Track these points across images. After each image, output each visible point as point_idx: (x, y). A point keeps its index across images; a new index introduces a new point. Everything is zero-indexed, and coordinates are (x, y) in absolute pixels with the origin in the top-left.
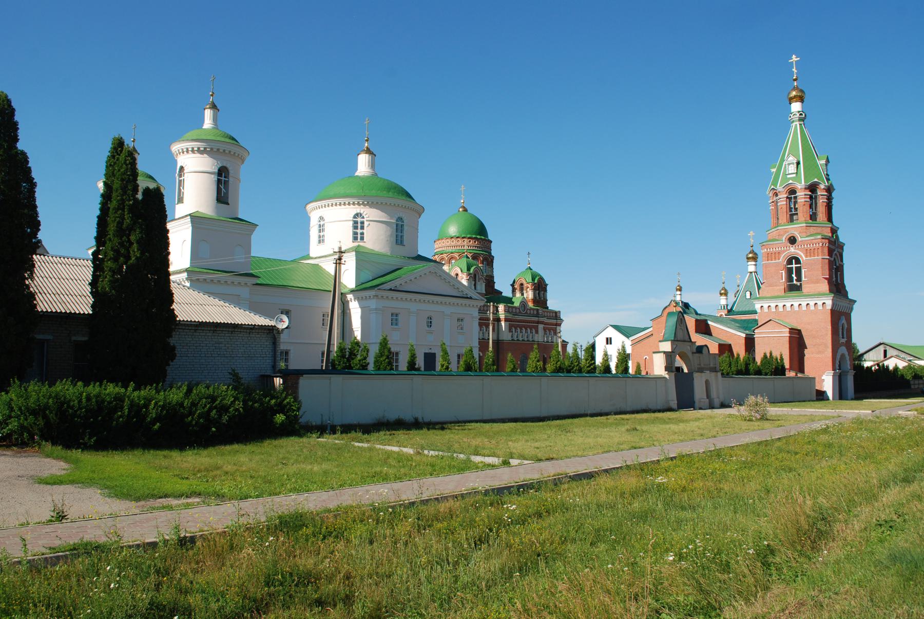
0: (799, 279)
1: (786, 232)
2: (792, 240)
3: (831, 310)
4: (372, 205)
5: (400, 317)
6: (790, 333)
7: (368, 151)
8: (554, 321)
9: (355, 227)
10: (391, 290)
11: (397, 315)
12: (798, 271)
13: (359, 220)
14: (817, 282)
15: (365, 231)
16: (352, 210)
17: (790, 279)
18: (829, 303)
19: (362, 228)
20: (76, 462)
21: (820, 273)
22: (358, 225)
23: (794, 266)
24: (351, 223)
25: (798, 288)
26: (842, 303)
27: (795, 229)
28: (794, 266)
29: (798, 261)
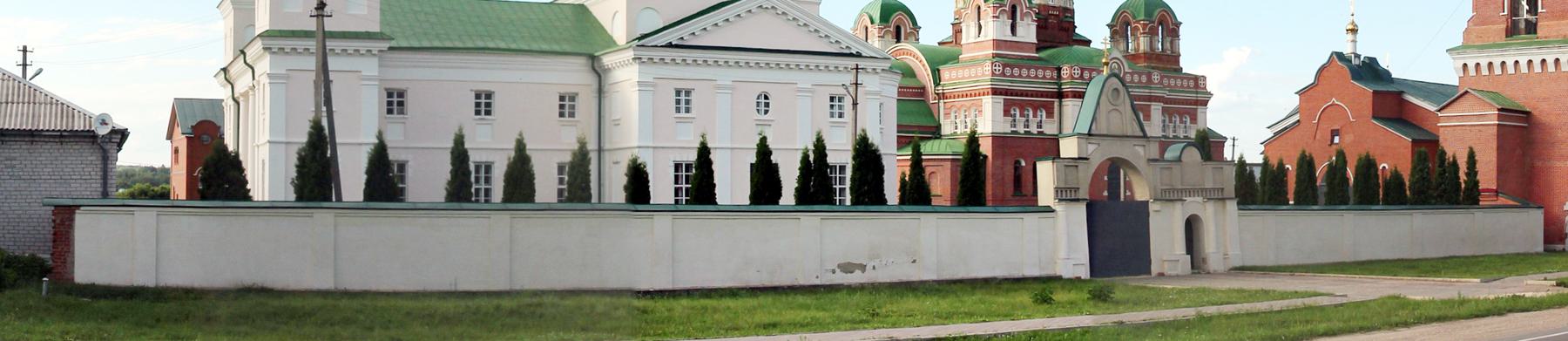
5: (693, 97)
6: (1500, 117)
8: (1192, 96)
10: (670, 45)
11: (688, 93)
25: (1531, 28)
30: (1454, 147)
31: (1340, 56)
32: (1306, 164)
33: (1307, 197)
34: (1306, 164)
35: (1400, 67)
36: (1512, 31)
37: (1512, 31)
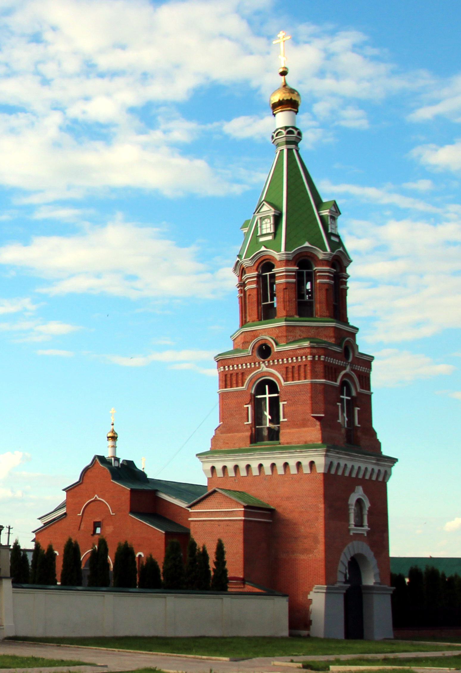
0: (275, 418)
1: (255, 337)
2: (264, 351)
3: (327, 476)
6: (246, 514)
12: (274, 403)
14: (304, 424)
17: (258, 418)
18: (320, 461)
20: (84, 112)
21: (308, 408)
23: (267, 396)
25: (274, 435)
26: (356, 464)
27: (267, 330)
28: (267, 396)
29: (273, 389)
30: (204, 540)
31: (102, 459)
32: (72, 550)
33: (73, 579)
34: (72, 550)
35: (157, 467)
36: (256, 438)
37: (256, 438)
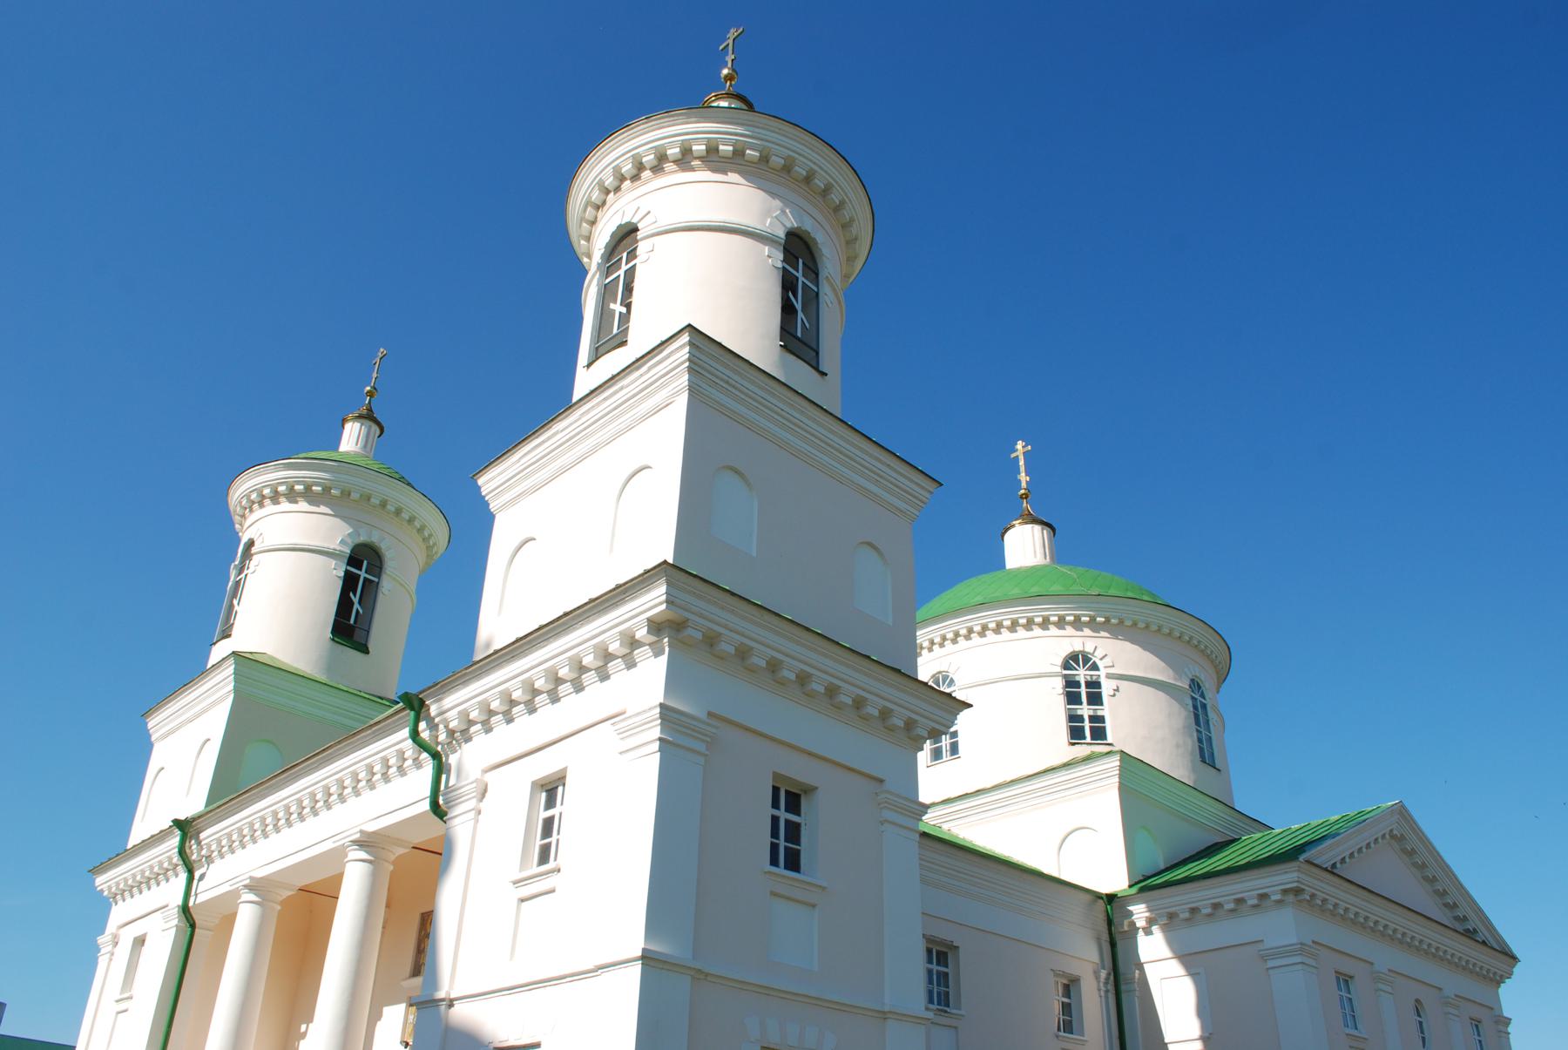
4: (1119, 628)
7: (369, 416)
9: (1072, 698)
13: (1082, 675)
15: (1105, 710)
16: (1053, 646)
19: (1095, 699)
22: (1081, 690)
24: (1059, 683)
